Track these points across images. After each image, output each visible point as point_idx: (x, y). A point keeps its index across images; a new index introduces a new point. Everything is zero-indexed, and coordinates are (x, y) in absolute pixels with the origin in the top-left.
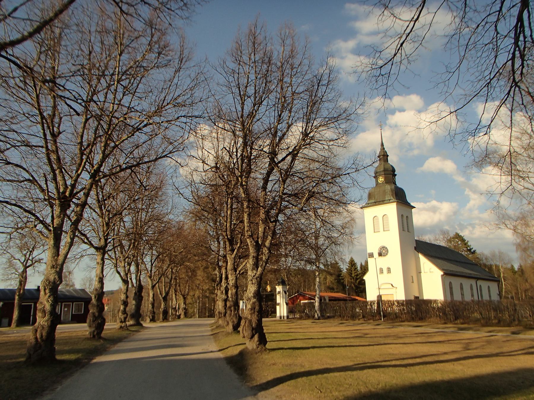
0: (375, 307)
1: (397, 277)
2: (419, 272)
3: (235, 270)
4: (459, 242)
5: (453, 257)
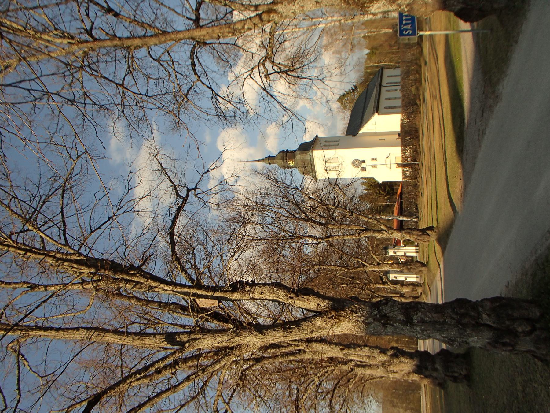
0: (407, 169)
1: (380, 152)
2: (376, 133)
3: (378, 264)
4: (346, 98)
5: (361, 105)
